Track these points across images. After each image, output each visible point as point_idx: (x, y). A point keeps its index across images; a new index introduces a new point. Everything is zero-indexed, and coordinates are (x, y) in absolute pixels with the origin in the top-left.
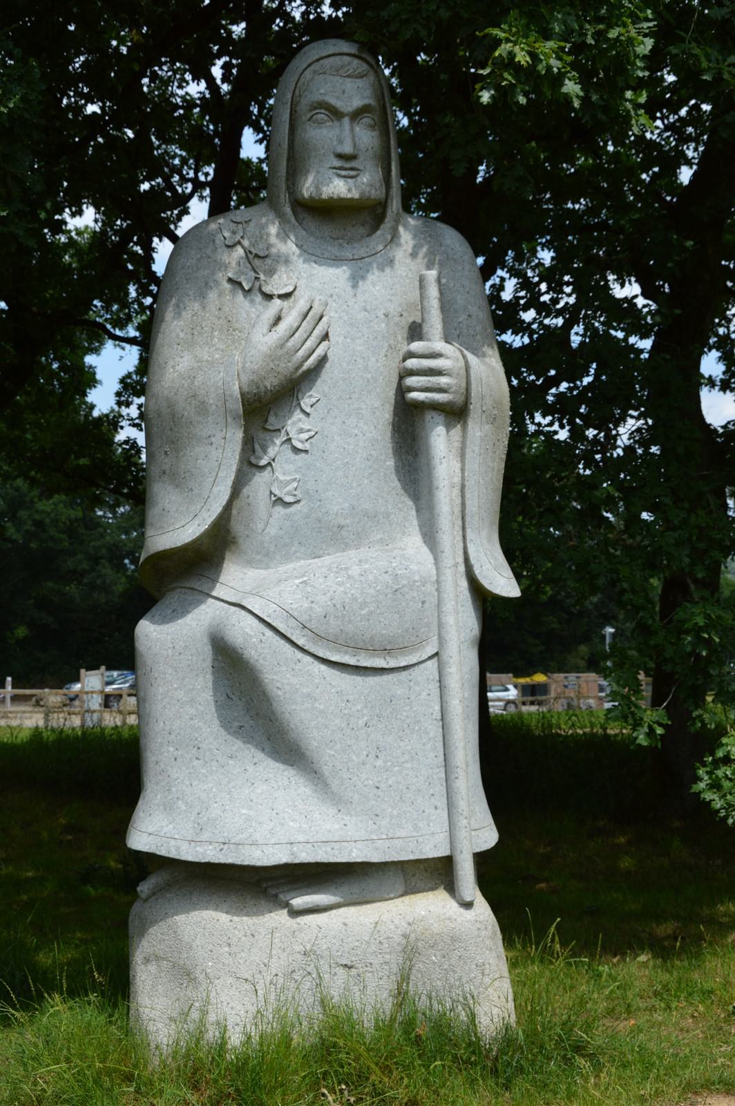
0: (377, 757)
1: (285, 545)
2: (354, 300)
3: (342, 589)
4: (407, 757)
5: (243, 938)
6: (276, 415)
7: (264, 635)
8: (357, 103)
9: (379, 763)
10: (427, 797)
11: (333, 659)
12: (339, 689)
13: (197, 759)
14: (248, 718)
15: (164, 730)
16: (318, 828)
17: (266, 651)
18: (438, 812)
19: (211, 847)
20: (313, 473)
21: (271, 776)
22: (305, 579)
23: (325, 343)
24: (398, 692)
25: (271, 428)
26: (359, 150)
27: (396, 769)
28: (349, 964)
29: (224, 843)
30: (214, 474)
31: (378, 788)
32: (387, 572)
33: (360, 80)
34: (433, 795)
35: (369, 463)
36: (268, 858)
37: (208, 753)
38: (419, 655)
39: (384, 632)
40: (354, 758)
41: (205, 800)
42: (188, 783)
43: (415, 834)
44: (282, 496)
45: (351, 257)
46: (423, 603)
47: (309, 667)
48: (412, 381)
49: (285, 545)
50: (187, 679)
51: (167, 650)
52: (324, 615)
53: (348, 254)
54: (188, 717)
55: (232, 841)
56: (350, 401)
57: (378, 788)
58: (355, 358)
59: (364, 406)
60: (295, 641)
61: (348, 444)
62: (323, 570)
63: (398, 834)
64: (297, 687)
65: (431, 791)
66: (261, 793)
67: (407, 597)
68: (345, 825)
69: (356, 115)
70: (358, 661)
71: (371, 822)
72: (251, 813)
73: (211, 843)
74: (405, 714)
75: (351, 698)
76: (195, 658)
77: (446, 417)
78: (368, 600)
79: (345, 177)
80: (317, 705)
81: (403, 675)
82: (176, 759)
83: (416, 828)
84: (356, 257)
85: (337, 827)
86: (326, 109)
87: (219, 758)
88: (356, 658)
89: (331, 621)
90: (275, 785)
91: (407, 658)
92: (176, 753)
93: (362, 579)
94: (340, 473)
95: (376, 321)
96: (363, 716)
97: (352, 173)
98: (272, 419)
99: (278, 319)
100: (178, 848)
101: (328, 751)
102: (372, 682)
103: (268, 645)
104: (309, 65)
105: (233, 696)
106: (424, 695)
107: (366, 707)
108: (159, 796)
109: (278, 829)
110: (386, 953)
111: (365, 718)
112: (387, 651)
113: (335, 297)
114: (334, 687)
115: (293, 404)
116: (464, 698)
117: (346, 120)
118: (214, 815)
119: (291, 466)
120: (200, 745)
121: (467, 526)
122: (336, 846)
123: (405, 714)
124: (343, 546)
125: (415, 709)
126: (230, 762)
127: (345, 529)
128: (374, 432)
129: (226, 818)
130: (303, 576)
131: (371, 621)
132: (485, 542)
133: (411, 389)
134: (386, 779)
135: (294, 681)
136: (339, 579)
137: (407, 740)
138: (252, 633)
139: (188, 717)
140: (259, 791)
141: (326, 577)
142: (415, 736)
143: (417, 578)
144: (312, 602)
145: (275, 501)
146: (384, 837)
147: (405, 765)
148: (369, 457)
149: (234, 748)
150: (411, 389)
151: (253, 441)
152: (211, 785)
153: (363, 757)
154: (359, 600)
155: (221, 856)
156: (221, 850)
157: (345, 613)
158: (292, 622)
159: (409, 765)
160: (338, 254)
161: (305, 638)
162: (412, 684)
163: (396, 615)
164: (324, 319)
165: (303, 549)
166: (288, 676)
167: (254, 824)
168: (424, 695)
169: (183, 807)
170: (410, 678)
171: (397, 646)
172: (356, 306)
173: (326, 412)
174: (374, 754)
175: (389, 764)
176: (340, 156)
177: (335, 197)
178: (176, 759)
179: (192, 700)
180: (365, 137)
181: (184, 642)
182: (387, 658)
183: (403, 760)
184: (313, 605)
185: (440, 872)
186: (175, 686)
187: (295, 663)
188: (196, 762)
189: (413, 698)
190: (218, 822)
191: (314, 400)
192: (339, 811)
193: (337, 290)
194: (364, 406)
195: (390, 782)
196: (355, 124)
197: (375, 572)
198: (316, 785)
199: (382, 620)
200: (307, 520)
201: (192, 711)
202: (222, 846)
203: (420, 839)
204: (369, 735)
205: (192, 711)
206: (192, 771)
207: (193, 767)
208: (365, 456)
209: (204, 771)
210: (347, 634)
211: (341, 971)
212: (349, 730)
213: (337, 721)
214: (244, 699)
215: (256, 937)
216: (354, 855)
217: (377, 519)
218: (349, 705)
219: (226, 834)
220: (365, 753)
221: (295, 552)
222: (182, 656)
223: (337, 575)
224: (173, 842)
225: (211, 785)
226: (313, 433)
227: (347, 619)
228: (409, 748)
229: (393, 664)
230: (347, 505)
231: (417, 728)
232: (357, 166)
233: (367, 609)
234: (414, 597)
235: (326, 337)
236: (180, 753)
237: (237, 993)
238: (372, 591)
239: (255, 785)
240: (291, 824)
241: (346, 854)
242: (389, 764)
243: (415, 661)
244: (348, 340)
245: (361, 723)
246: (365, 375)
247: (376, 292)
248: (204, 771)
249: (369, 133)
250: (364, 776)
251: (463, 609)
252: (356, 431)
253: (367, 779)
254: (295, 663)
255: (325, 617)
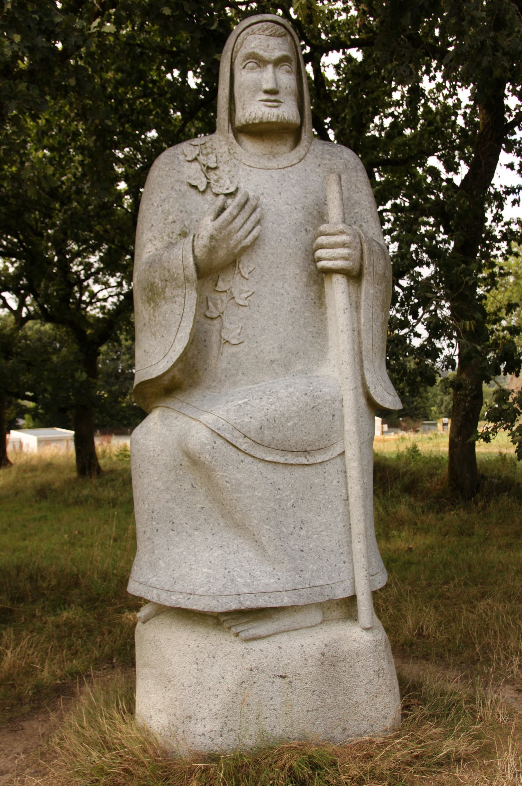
0: (301, 528)
1: (232, 375)
2: (279, 197)
3: (273, 407)
4: (323, 527)
5: (207, 659)
6: (223, 280)
7: (215, 443)
8: (277, 54)
9: (303, 533)
10: (338, 555)
11: (267, 459)
12: (273, 481)
13: (172, 530)
14: (207, 502)
15: (148, 509)
16: (259, 582)
17: (217, 455)
18: (346, 565)
19: (181, 596)
20: (251, 322)
21: (225, 543)
22: (246, 400)
23: (259, 227)
24: (316, 481)
25: (220, 290)
26: (280, 88)
27: (315, 536)
28: (284, 675)
29: (191, 594)
30: (178, 324)
31: (302, 551)
32: (306, 394)
33: (280, 38)
34: (342, 553)
35: (292, 315)
36: (222, 606)
37: (180, 526)
38: (330, 453)
39: (305, 438)
40: (284, 530)
41: (178, 560)
42: (166, 548)
43: (329, 582)
44: (229, 340)
45: (277, 167)
46: (333, 416)
47: (250, 466)
48: (320, 253)
49: (232, 375)
50: (164, 474)
51: (149, 452)
52: (260, 426)
53: (274, 165)
54: (164, 501)
55: (196, 593)
56: (278, 269)
57: (302, 551)
58: (280, 238)
59: (288, 273)
60: (239, 447)
61: (277, 300)
62: (260, 393)
63: (317, 583)
64: (242, 480)
65: (341, 551)
66: (218, 557)
67: (321, 412)
68: (279, 579)
69: (278, 63)
70: (286, 460)
71: (297, 576)
72: (210, 571)
73: (181, 593)
74: (321, 497)
75: (281, 487)
76: (168, 459)
77: (348, 281)
78: (292, 415)
79: (270, 107)
80: (256, 493)
81: (320, 469)
82: (157, 531)
83: (330, 577)
84: (280, 167)
85: (272, 581)
86: (253, 58)
87: (188, 531)
88: (285, 457)
89: (266, 432)
90: (227, 550)
91: (322, 456)
92: (157, 526)
93: (288, 399)
94: (271, 322)
95: (295, 211)
96: (291, 499)
97: (275, 104)
98: (221, 284)
99: (223, 209)
100: (158, 596)
101: (265, 526)
102: (296, 475)
103: (218, 450)
104: (244, 30)
105: (196, 486)
106: (335, 483)
107: (293, 493)
108: (147, 556)
109: (229, 584)
110: (309, 666)
111: (293, 501)
112: (306, 452)
113: (265, 195)
114: (268, 479)
115: (236, 272)
116: (364, 483)
117: (270, 67)
118: (184, 572)
119: (235, 318)
120: (175, 521)
121: (364, 358)
122: (273, 595)
123: (321, 497)
124: (274, 375)
125: (328, 492)
126: (195, 533)
127: (276, 362)
128: (296, 291)
129: (192, 575)
130: (245, 398)
131: (295, 431)
132: (377, 370)
133: (320, 259)
134: (308, 544)
135: (239, 476)
136: (271, 400)
137: (323, 515)
138: (207, 442)
139: (164, 501)
140: (216, 555)
141: (261, 399)
142: (329, 512)
143: (328, 398)
144: (251, 418)
145: (225, 343)
146: (307, 586)
147: (322, 533)
148: (292, 310)
149: (198, 523)
150: (320, 259)
151: (207, 301)
152: (182, 550)
153: (291, 529)
154: (286, 416)
155: (188, 604)
156: (189, 599)
157: (275, 425)
158: (237, 434)
159: (325, 533)
160: (266, 164)
161: (246, 444)
162: (326, 475)
163: (314, 426)
164: (258, 210)
165: (245, 377)
166: (234, 472)
167: (212, 581)
168: (335, 483)
169: (163, 565)
170: (324, 470)
171: (315, 448)
172: (281, 201)
173: (260, 277)
174: (299, 526)
175: (310, 533)
176: (266, 92)
177: (264, 120)
178: (157, 531)
179: (168, 489)
180: (286, 80)
181: (161, 446)
182: (308, 457)
183: (320, 530)
184: (252, 420)
185: (348, 606)
186: (155, 478)
187: (240, 463)
188: (171, 533)
189: (326, 485)
190: (186, 577)
191: (251, 269)
192: (274, 569)
193: (266, 190)
194: (288, 273)
195: (311, 546)
196: (277, 70)
197: (298, 394)
198: (257, 551)
199: (303, 429)
200: (248, 357)
201: (168, 496)
202: (189, 596)
203: (334, 586)
204: (295, 513)
205: (168, 496)
206: (168, 539)
207: (170, 536)
208: (289, 309)
209: (177, 539)
210: (277, 441)
211: (278, 680)
212: (280, 511)
213: (272, 504)
214: (204, 488)
215: (216, 658)
216: (285, 601)
217: (299, 355)
218: (280, 492)
219: (192, 587)
220: (292, 526)
221: (240, 380)
222: (160, 457)
223: (270, 397)
224: (155, 591)
225: (182, 550)
226: (250, 293)
227: (277, 429)
228: (325, 520)
229: (311, 461)
230: (276, 345)
231: (330, 506)
232: (278, 99)
233: (292, 422)
234: (326, 412)
235: (258, 222)
236: (160, 526)
237: (204, 697)
238: (295, 408)
239: (213, 550)
240: (239, 579)
241: (280, 601)
242: (310, 533)
243: (328, 458)
244: (275, 225)
245: (289, 504)
246: (288, 251)
247: (295, 192)
248: (177, 539)
249: (287, 76)
250: (292, 543)
251: (362, 419)
252: (282, 291)
253: (294, 545)
254: (240, 463)
255: (261, 428)
